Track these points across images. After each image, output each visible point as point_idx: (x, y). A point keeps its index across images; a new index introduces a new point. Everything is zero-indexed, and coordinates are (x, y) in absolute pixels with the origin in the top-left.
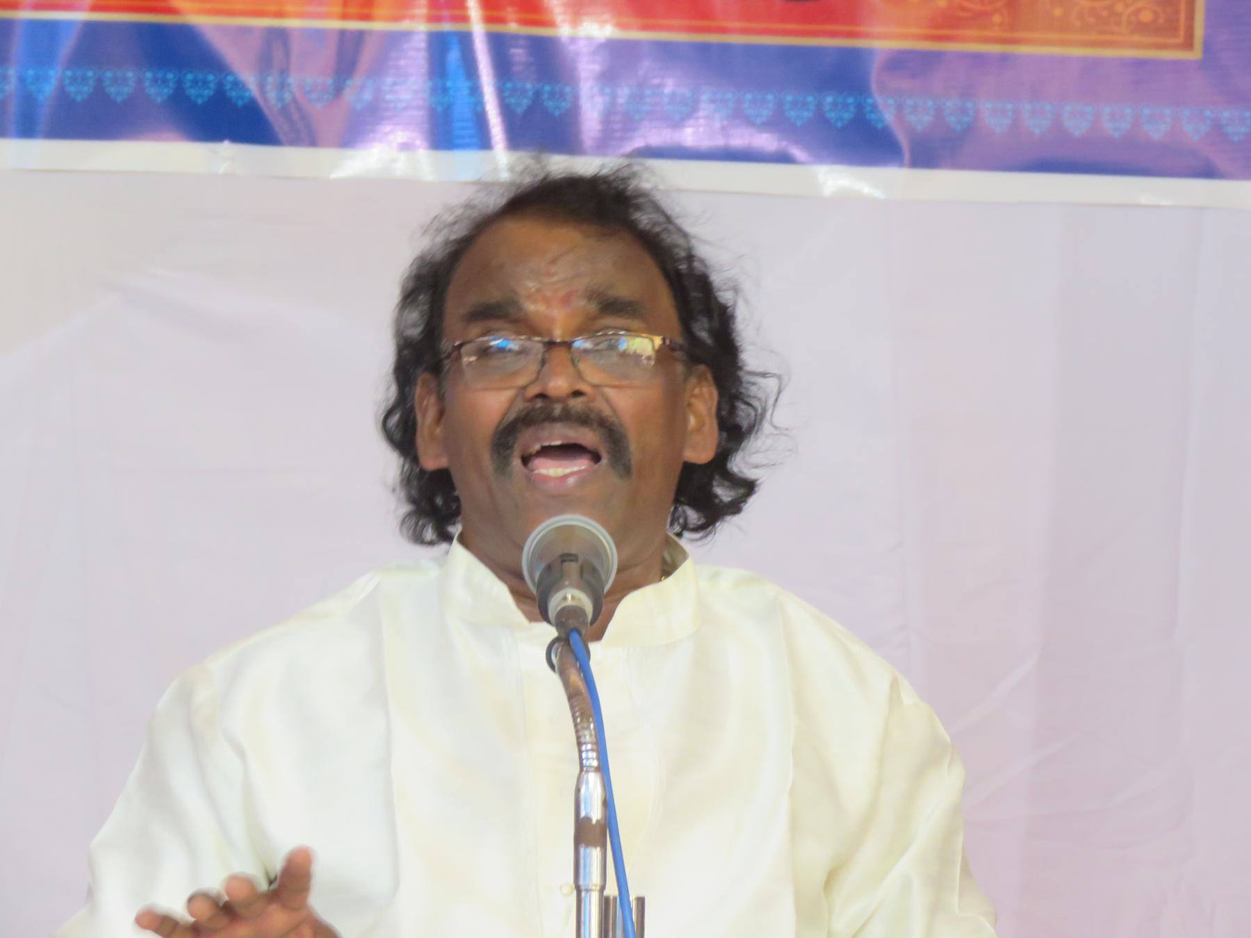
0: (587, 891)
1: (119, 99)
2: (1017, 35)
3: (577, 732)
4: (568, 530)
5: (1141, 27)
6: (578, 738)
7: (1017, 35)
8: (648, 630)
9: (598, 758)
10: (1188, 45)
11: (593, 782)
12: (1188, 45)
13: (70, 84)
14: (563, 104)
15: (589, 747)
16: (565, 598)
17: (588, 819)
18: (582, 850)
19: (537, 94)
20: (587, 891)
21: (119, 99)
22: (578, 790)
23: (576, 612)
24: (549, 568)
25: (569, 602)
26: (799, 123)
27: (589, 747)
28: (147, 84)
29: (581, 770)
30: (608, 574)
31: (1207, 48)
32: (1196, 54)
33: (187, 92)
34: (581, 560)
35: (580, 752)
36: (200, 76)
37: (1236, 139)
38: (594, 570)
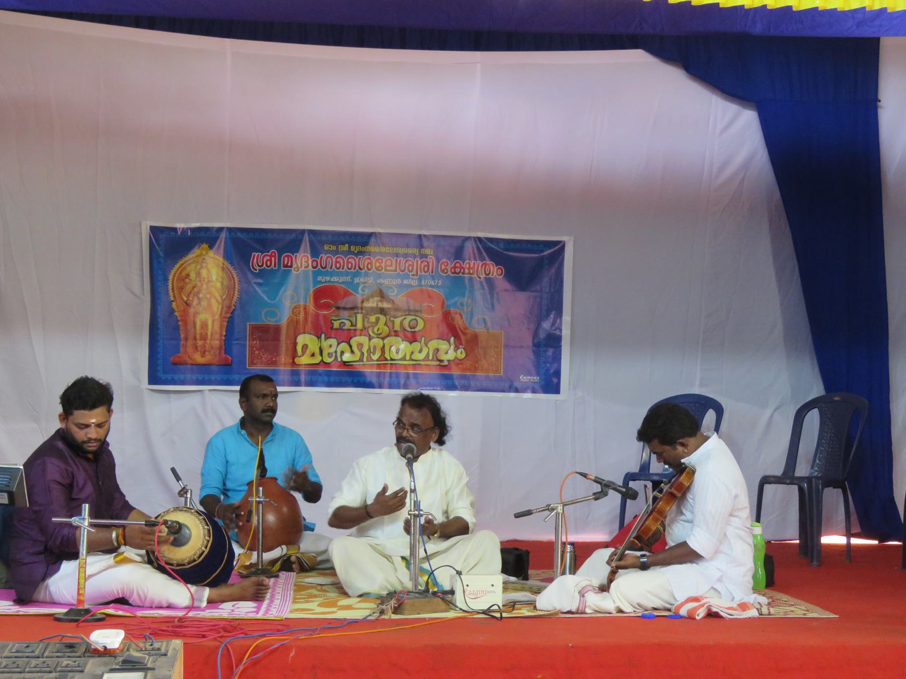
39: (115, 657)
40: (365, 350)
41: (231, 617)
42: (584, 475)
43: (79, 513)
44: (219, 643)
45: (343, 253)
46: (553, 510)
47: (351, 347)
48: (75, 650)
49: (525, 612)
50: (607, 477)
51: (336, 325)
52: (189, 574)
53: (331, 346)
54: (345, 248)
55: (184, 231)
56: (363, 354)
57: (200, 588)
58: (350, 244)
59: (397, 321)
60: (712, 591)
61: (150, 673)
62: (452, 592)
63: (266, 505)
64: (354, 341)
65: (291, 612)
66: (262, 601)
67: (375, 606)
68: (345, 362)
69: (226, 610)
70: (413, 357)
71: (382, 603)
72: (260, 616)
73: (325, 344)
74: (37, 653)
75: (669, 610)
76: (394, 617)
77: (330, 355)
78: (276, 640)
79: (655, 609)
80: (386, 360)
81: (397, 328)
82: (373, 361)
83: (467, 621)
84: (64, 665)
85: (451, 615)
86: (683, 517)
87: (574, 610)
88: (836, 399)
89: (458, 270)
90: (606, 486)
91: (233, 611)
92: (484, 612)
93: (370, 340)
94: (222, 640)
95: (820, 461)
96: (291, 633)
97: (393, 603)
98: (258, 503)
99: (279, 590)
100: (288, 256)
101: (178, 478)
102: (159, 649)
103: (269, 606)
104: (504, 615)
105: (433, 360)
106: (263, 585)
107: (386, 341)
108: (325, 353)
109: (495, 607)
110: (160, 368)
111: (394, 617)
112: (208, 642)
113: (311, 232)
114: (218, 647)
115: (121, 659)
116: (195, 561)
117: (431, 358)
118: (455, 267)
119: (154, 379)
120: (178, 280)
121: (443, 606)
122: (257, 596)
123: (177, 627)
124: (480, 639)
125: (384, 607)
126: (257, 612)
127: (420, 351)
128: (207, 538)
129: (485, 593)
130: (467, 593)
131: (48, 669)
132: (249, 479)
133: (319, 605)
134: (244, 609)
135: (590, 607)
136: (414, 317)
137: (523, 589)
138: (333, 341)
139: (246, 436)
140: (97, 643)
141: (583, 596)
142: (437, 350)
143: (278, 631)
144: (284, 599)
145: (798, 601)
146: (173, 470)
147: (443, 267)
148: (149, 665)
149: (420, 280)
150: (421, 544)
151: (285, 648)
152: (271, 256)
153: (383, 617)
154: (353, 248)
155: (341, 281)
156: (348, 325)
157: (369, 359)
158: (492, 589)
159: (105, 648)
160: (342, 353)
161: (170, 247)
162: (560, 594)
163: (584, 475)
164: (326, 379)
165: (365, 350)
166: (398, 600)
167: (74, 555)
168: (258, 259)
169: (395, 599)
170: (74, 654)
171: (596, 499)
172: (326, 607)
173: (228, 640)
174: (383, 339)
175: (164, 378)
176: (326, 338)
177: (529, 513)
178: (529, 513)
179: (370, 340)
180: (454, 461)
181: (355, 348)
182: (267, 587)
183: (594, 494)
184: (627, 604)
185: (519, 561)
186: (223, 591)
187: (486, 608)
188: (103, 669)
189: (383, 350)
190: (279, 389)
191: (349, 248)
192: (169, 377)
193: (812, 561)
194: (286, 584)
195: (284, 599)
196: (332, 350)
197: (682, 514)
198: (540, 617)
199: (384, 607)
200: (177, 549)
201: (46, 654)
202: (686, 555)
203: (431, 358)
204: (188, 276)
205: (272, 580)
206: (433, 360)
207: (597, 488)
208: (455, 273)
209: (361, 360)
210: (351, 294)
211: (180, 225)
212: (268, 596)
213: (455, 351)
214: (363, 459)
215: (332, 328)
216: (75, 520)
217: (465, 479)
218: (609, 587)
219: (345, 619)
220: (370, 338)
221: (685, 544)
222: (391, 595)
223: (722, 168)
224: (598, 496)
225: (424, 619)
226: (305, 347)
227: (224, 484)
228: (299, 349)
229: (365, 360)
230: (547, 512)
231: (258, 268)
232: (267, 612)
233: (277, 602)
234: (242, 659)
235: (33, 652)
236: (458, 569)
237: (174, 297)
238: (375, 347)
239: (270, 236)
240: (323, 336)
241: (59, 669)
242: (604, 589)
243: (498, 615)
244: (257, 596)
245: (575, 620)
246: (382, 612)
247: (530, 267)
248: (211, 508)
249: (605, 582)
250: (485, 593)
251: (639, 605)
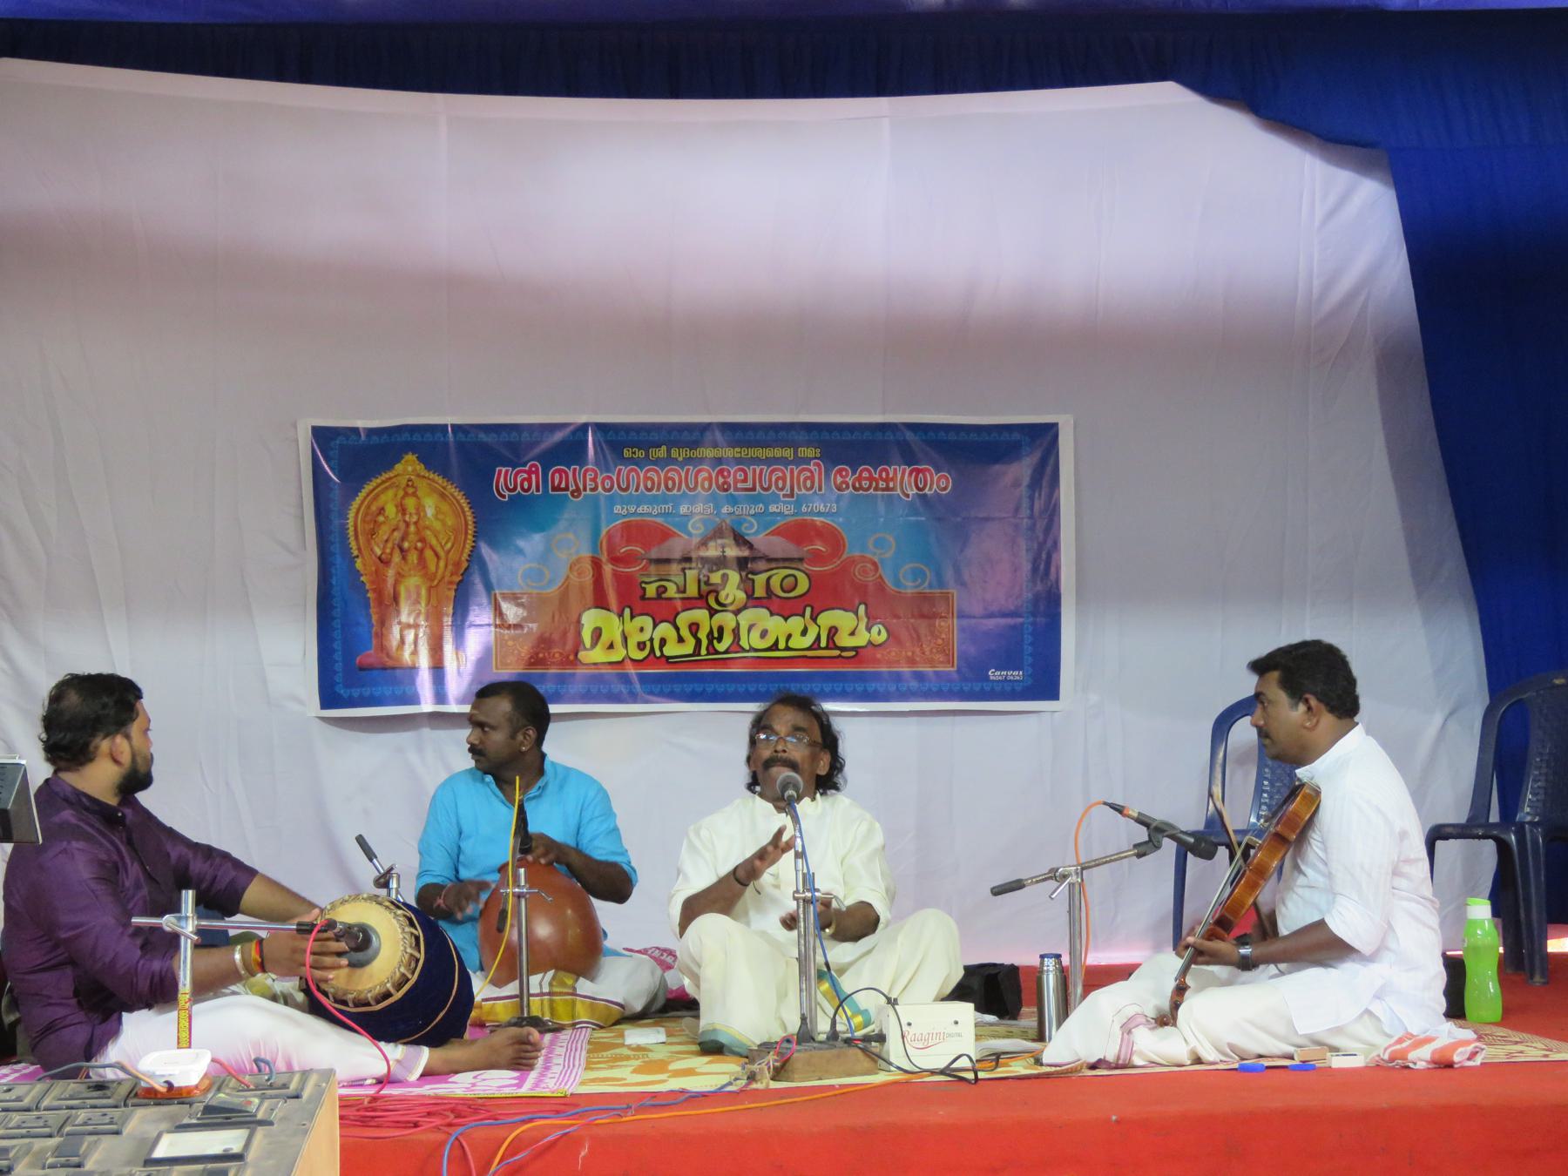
39: (191, 1104)
40: (703, 635)
41: (469, 1095)
42: (1119, 809)
43: (174, 907)
44: (439, 1136)
45: (657, 462)
46: (1065, 877)
47: (677, 629)
48: (108, 1093)
49: (1019, 1068)
50: (1158, 814)
51: (651, 591)
52: (382, 1022)
53: (642, 630)
54: (662, 452)
55: (372, 432)
56: (698, 642)
57: (412, 1049)
58: (671, 444)
59: (760, 580)
60: (1366, 1017)
61: (261, 1131)
62: (881, 1038)
63: (535, 905)
64: (684, 619)
65: (582, 1083)
66: (531, 1067)
67: (738, 1069)
68: (668, 658)
69: (462, 1085)
70: (791, 644)
71: (752, 1061)
72: (524, 1091)
73: (632, 626)
74: (26, 1102)
75: (1292, 1058)
76: (774, 1085)
77: (641, 646)
78: (552, 1127)
79: (1260, 1056)
80: (744, 650)
81: (760, 592)
82: (717, 652)
83: (911, 1088)
84: (79, 1121)
85: (880, 1078)
86: (1301, 880)
87: (1111, 1057)
88: (1557, 682)
89: (865, 484)
90: (1156, 831)
91: (474, 1085)
92: (942, 1072)
93: (711, 616)
94: (450, 1130)
95: (1534, 794)
96: (576, 1116)
97: (771, 1058)
98: (519, 896)
99: (559, 1050)
100: (558, 471)
101: (370, 855)
102: (285, 1086)
103: (542, 1075)
104: (981, 1075)
106: (529, 1043)
107: (740, 617)
108: (632, 643)
109: (964, 1063)
110: (338, 678)
111: (774, 1085)
112: (424, 1136)
113: (601, 428)
114: (442, 1144)
115: (201, 1106)
116: (387, 995)
117: (823, 643)
118: (860, 479)
119: (329, 698)
120: (364, 521)
121: (866, 1063)
122: (521, 1059)
123: (366, 1109)
124: (940, 1114)
125: (755, 1067)
126: (519, 1086)
127: (804, 632)
128: (408, 929)
129: (943, 1037)
130: (908, 1038)
131: (47, 1130)
132: (499, 862)
133: (634, 1072)
134: (497, 1082)
135: (1141, 1054)
136: (792, 595)
137: (1009, 1035)
138: (646, 621)
139: (494, 786)
140: (152, 1076)
141: (1130, 1032)
142: (833, 631)
143: (558, 1112)
144: (569, 1066)
145: (1526, 1036)
146: (361, 841)
147: (839, 480)
148: (260, 1116)
149: (798, 504)
150: (819, 951)
151: (567, 1143)
152: (529, 473)
153: (754, 1086)
154: (674, 453)
155: (655, 512)
156: (672, 591)
157: (712, 650)
158: (955, 1029)
159: (170, 1085)
160: (663, 642)
161: (350, 460)
162: (1085, 1034)
163: (1119, 809)
165: (703, 635)
166: (778, 1054)
167: (160, 994)
168: (505, 479)
169: (783, 1055)
170: (104, 1101)
171: (1139, 856)
172: (650, 1072)
173: (461, 1129)
174: (737, 613)
175: (346, 696)
176: (632, 617)
177: (1017, 885)
178: (1017, 885)
179: (711, 616)
181: (685, 633)
182: (536, 1048)
183: (1136, 846)
184: (1208, 1046)
185: (993, 990)
186: (452, 1052)
187: (942, 1065)
188: (164, 1126)
189: (736, 632)
190: (553, 709)
191: (669, 452)
192: (356, 693)
193: (1532, 976)
194: (572, 1041)
195: (569, 1066)
196: (645, 637)
197: (1301, 872)
198: (1047, 1076)
199: (755, 1067)
200: (368, 969)
201: (45, 1103)
202: (1320, 947)
203: (823, 643)
204: (381, 510)
205: (548, 1037)
206: (827, 648)
207: (1142, 834)
208: (861, 488)
210: (673, 535)
211: (361, 424)
212: (540, 1062)
213: (869, 629)
215: (643, 597)
216: (167, 922)
218: (1174, 1018)
219: (683, 1092)
220: (713, 612)
221: (1321, 924)
222: (766, 1047)
223: (1328, 286)
224: (1142, 850)
225: (832, 1087)
226: (597, 634)
227: (457, 871)
228: (587, 636)
229: (703, 651)
230: (1052, 884)
231: (507, 493)
232: (536, 1085)
233: (556, 1069)
234: (490, 1162)
235: (19, 1099)
236: (893, 996)
237: (359, 549)
238: (721, 630)
239: (525, 436)
240: (627, 612)
241: (68, 1129)
242: (1166, 1019)
243: (970, 1076)
244: (521, 1059)
245: (1108, 1074)
246: (752, 1077)
247: (995, 461)
248: (431, 913)
249: (1166, 1005)
250: (943, 1037)
251: (1232, 1047)
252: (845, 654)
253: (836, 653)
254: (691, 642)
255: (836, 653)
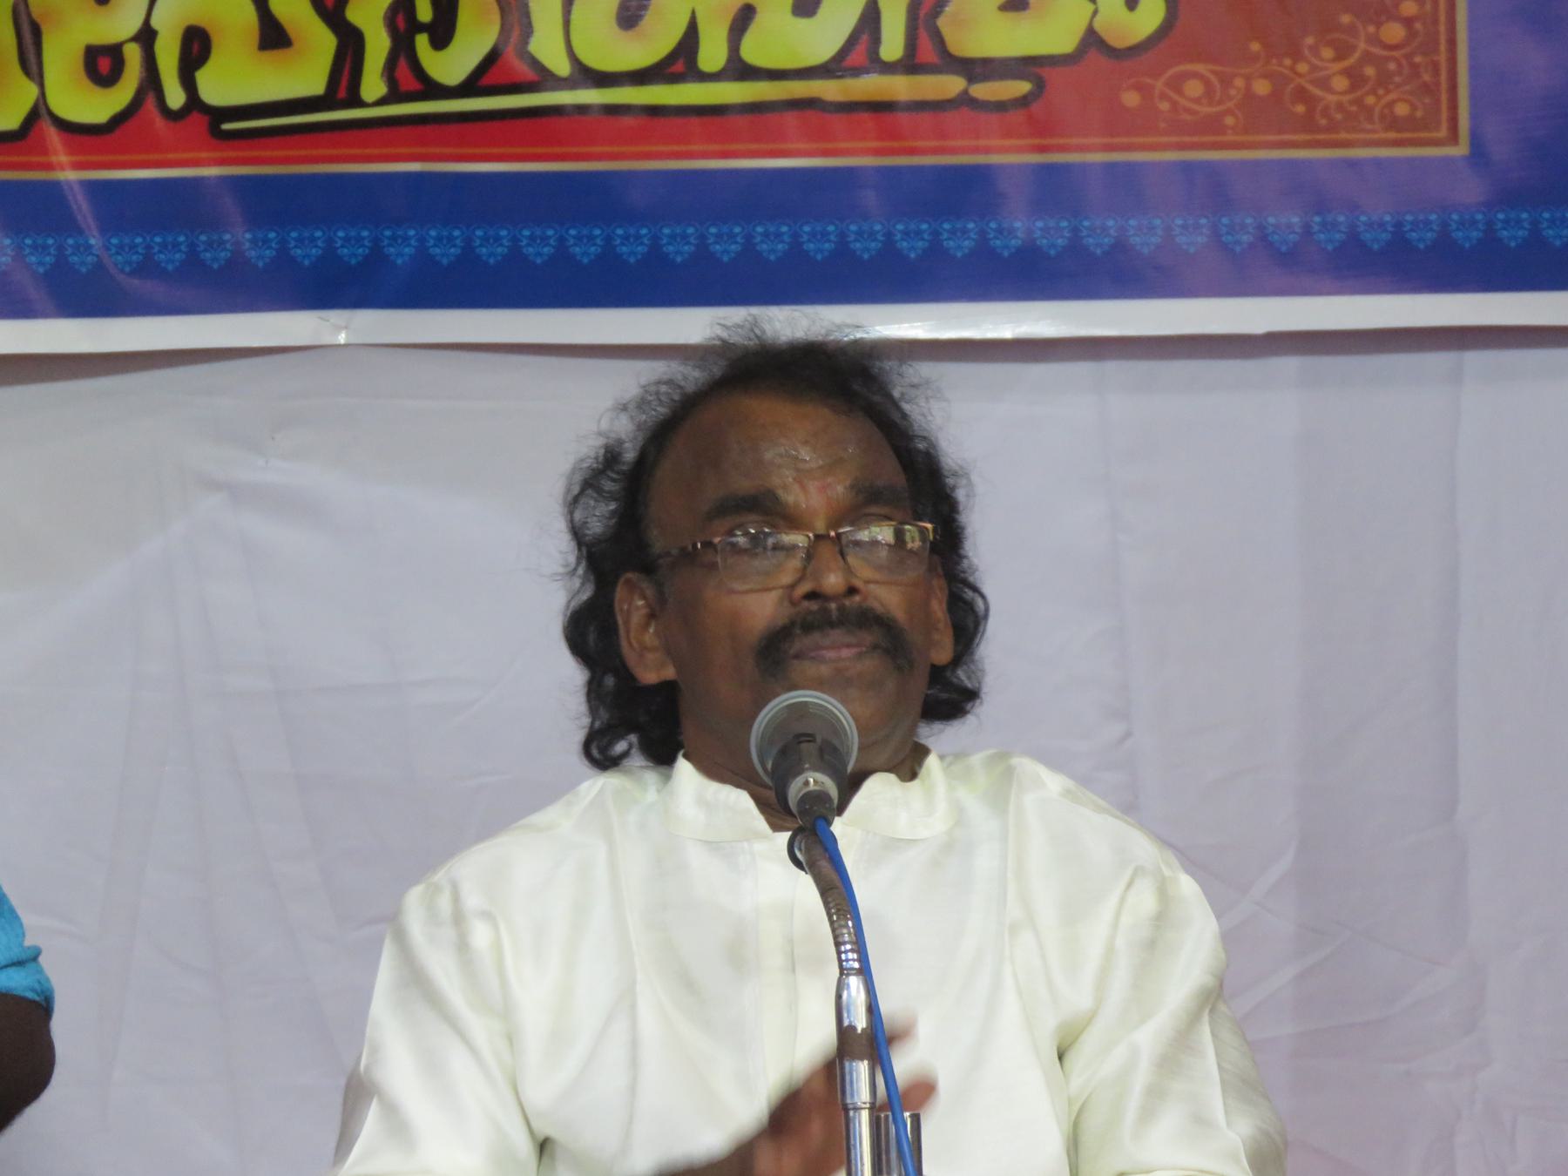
0: (857, 1109)
1: (726, 259)
2: (982, 143)
3: (833, 931)
4: (800, 710)
5: (1393, 123)
6: (835, 937)
7: (982, 143)
8: (881, 821)
9: (859, 960)
10: (1453, 138)
11: (855, 984)
12: (1453, 138)
13: (528, 245)
14: (1013, 242)
15: (848, 947)
16: (807, 783)
17: (852, 1028)
18: (847, 1064)
19: (889, 235)
20: (857, 1109)
21: (726, 259)
22: (839, 997)
23: (820, 797)
24: (783, 752)
25: (812, 786)
26: (170, 267)
27: (848, 947)
28: (1178, 231)
29: (841, 974)
30: (849, 754)
31: (1475, 137)
32: (1461, 150)
33: (898, 245)
34: (819, 740)
35: (839, 953)
36: (959, 225)
37: (1284, 249)
38: (835, 750)
56: (350, 44)
70: (754, 51)
77: (101, 64)
80: (543, 79)
105: (910, 64)
117: (892, 45)
157: (408, 78)
164: (240, 238)
180: (1103, 833)
203: (892, 45)
206: (910, 64)
209: (344, 80)
214: (470, 870)
217: (1197, 948)
229: (373, 85)
252: (982, 91)
253: (952, 85)
254: (320, 43)
255: (952, 85)
